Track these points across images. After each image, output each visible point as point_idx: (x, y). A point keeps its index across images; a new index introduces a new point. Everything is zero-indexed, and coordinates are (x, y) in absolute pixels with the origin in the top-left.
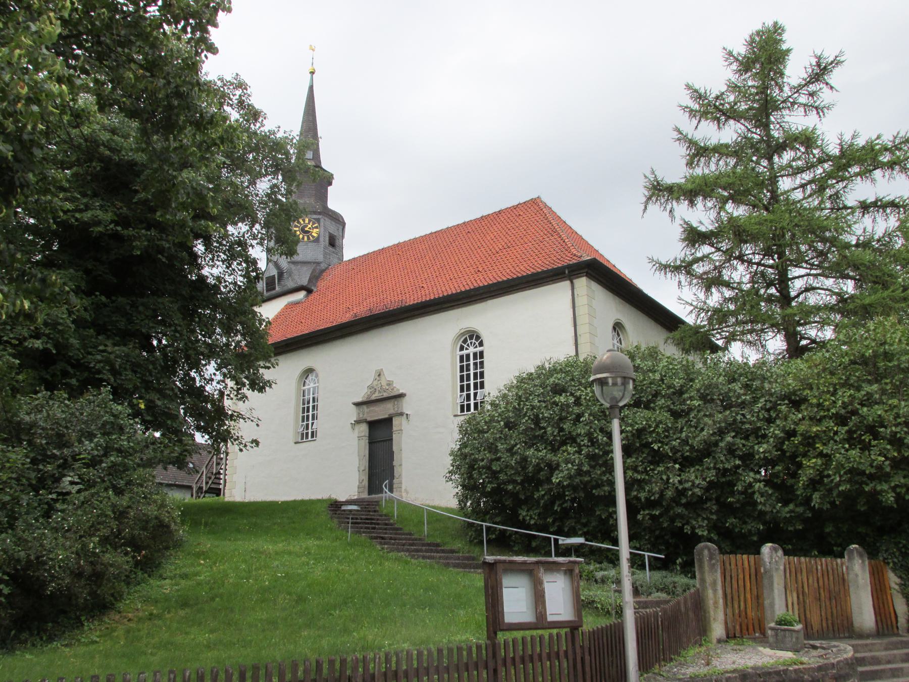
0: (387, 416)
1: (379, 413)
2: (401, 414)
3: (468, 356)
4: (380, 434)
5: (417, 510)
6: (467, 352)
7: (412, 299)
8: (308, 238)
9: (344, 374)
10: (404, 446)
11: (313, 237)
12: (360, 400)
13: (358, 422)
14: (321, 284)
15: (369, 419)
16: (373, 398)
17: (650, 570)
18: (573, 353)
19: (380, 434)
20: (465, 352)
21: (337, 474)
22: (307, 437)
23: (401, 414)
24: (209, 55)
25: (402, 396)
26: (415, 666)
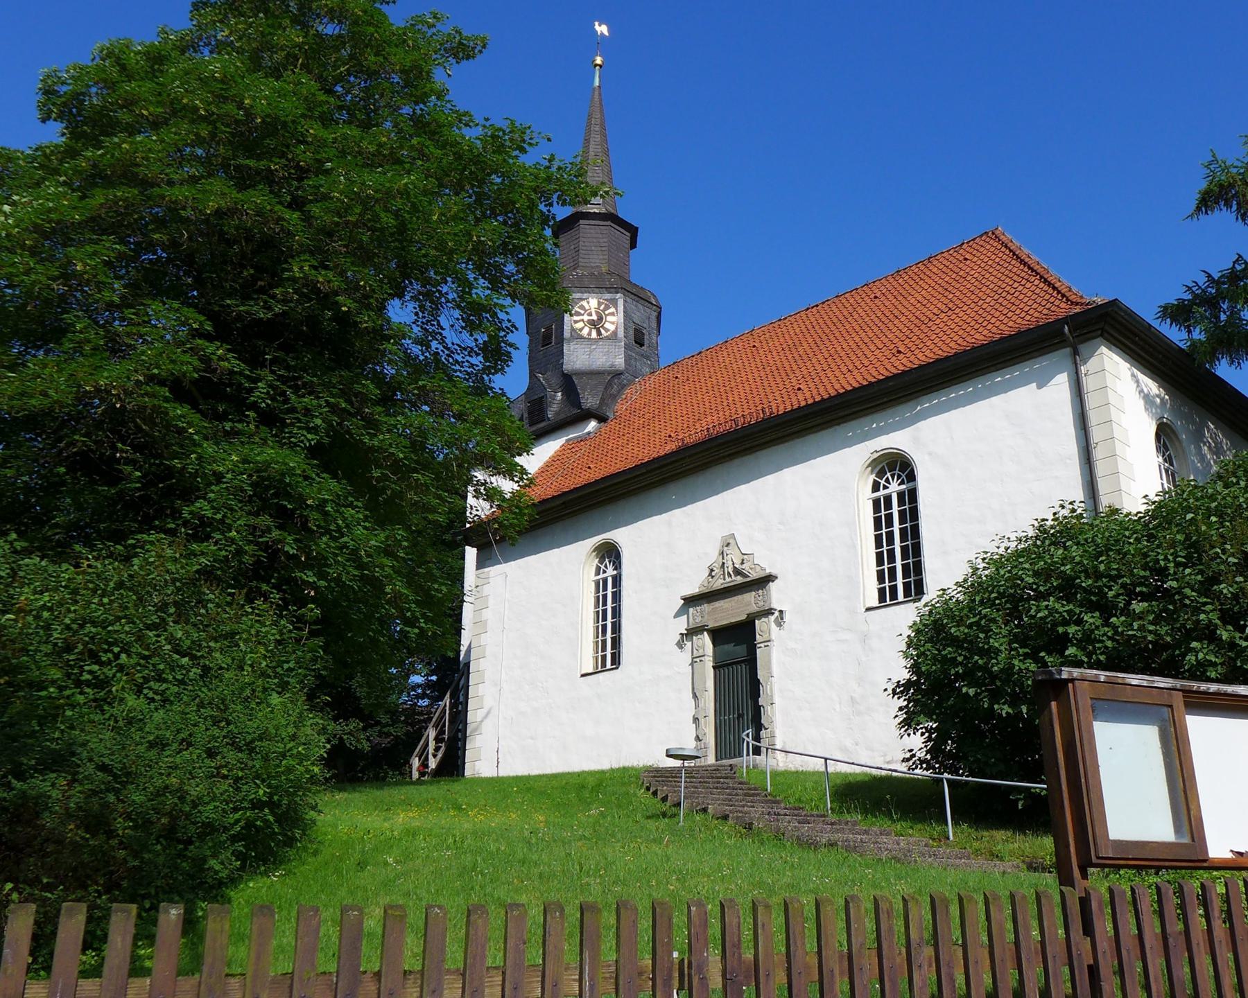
0: (744, 617)
1: (730, 611)
2: (769, 612)
3: (888, 499)
4: (735, 649)
5: (799, 776)
6: (886, 492)
7: (781, 404)
8: (599, 333)
9: (671, 548)
10: (775, 669)
11: (607, 330)
12: (693, 589)
13: (692, 632)
14: (621, 407)
15: (712, 625)
16: (719, 584)
17: (956, 822)
18: (1076, 493)
19: (735, 649)
20: (882, 492)
21: (655, 714)
22: (604, 664)
23: (769, 612)
24: (447, 98)
25: (769, 579)
26: (749, 955)
